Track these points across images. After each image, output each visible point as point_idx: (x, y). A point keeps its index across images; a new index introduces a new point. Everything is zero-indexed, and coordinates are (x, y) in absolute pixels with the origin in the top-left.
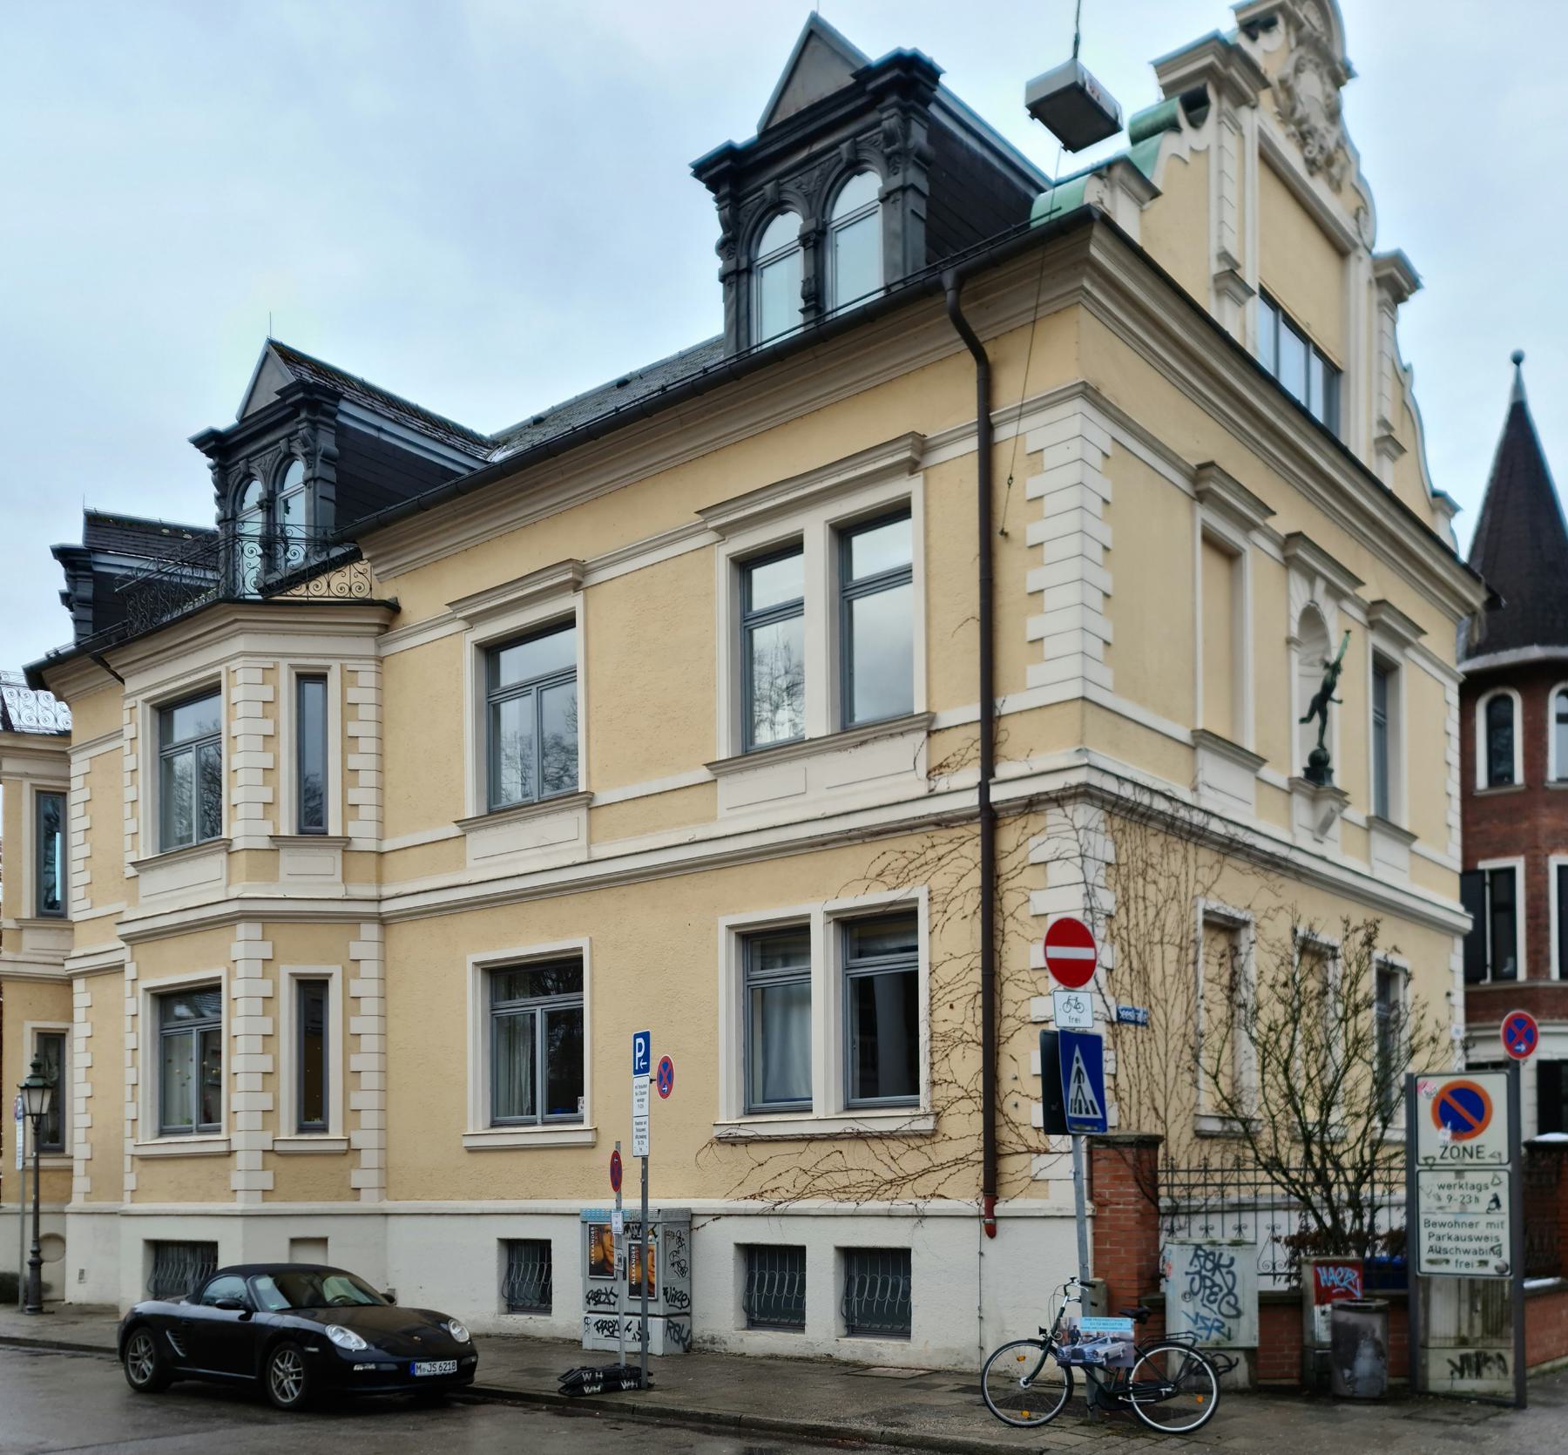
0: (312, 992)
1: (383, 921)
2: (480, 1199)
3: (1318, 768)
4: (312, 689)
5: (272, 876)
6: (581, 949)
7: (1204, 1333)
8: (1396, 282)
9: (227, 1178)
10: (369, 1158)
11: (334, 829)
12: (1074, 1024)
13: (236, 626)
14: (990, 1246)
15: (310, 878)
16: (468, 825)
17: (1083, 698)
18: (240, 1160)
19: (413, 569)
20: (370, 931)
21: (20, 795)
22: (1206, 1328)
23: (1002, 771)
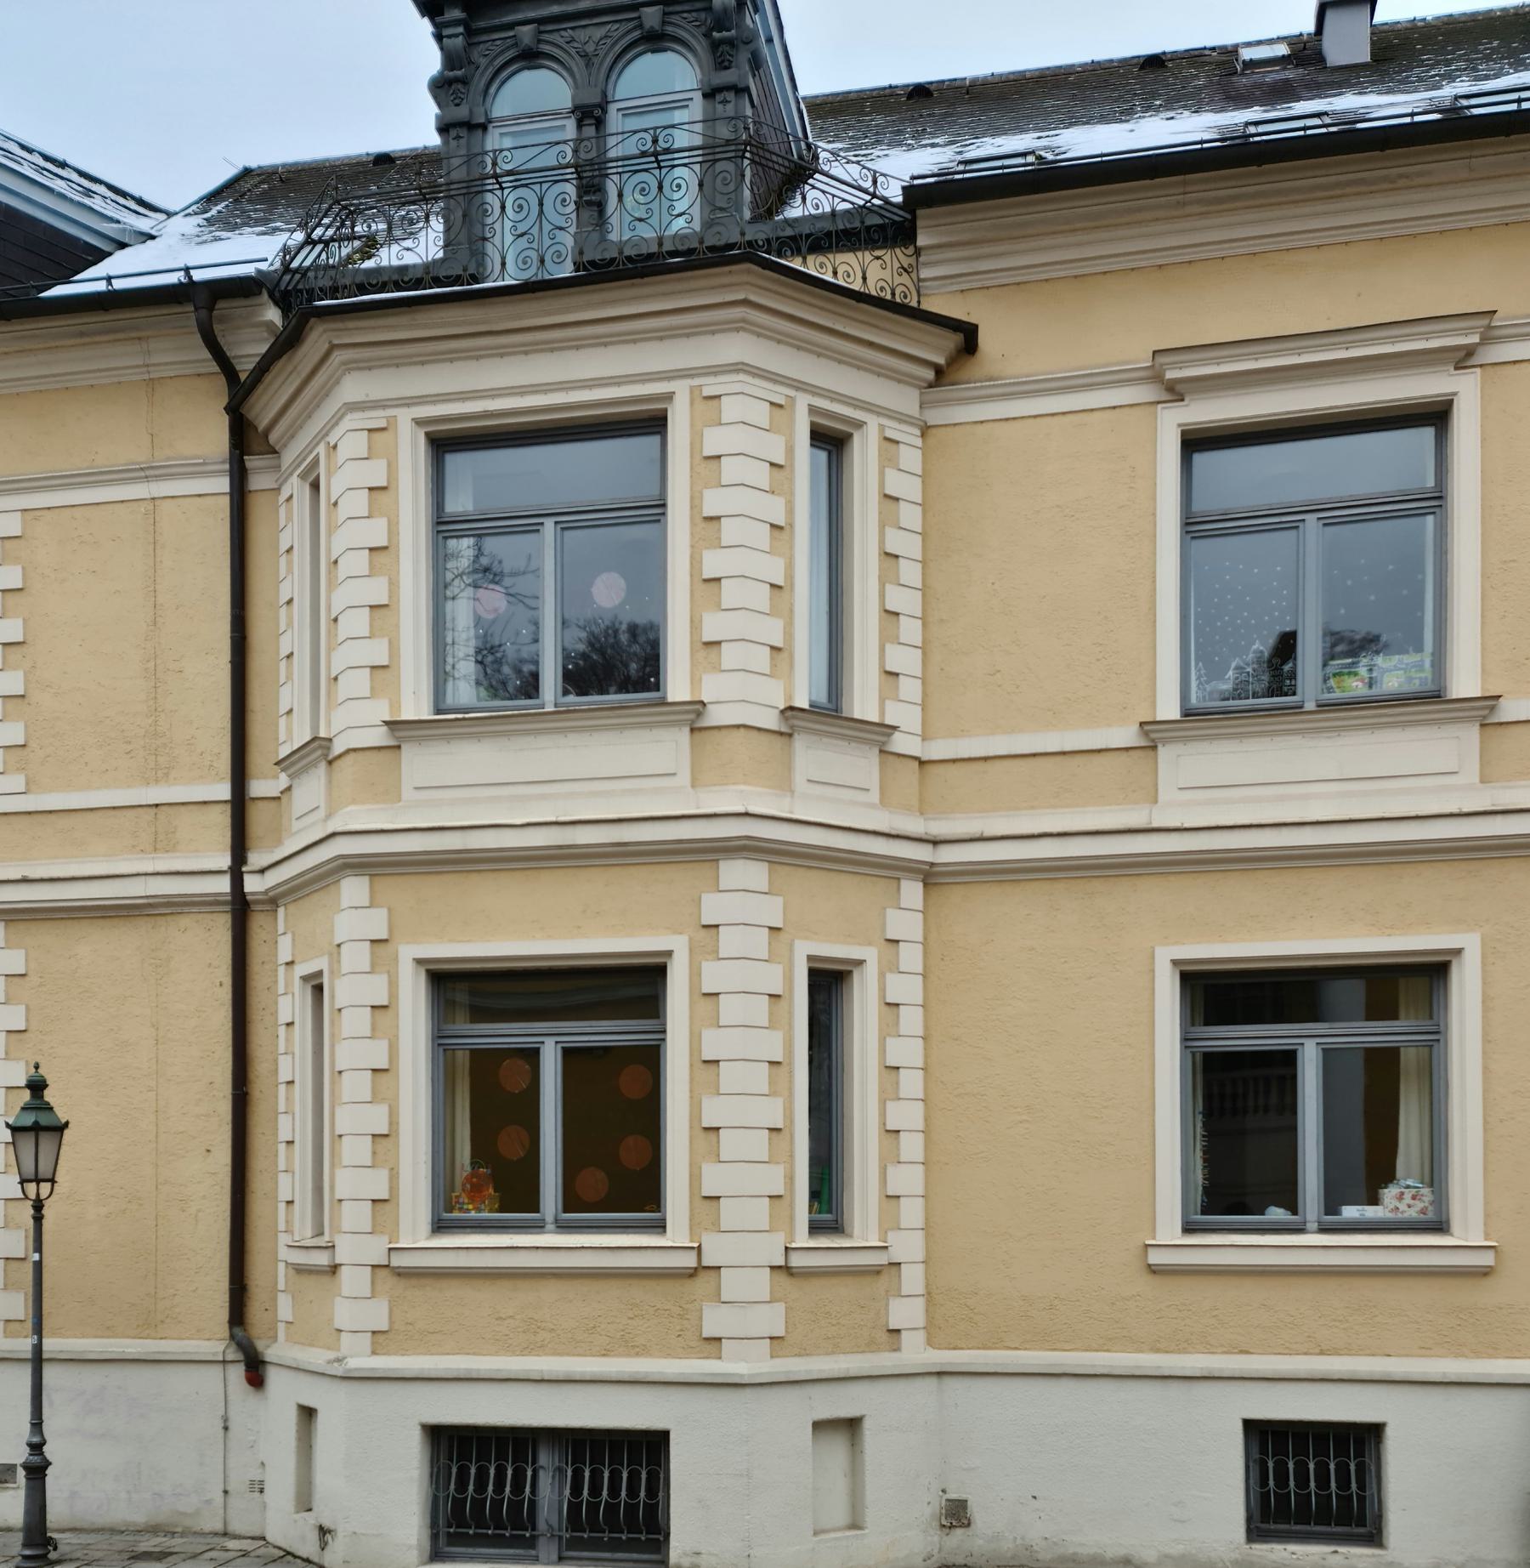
0: (828, 984)
1: (930, 876)
2: (1185, 1351)
5: (391, 793)
10: (913, 1278)
15: (831, 792)
16: (1153, 735)
19: (1016, 286)
20: (912, 891)
23: (256, 859)
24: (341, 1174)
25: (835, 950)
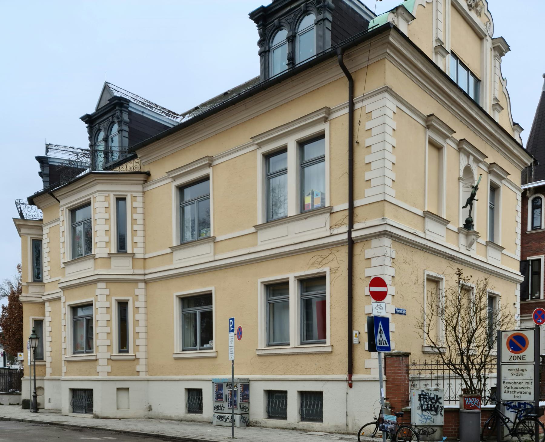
0: (123, 306)
1: (146, 282)
3: (469, 224)
4: (121, 202)
5: (109, 267)
6: (211, 291)
7: (425, 420)
8: (501, 48)
9: (96, 368)
10: (142, 361)
11: (129, 250)
12: (379, 314)
13: (96, 182)
14: (350, 391)
15: (121, 267)
17: (385, 200)
18: (100, 362)
19: (155, 162)
20: (142, 285)
21: (27, 241)
22: (425, 419)
23: (356, 226)
24: (98, 341)
25: (122, 298)
